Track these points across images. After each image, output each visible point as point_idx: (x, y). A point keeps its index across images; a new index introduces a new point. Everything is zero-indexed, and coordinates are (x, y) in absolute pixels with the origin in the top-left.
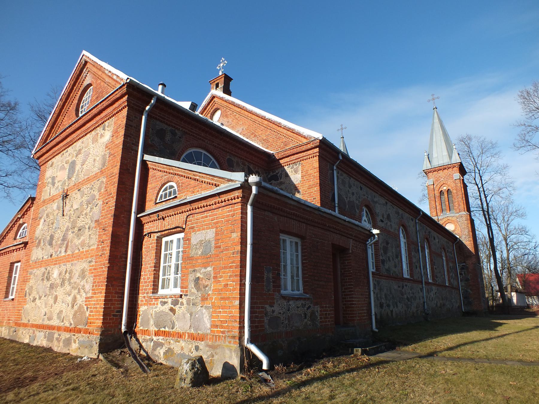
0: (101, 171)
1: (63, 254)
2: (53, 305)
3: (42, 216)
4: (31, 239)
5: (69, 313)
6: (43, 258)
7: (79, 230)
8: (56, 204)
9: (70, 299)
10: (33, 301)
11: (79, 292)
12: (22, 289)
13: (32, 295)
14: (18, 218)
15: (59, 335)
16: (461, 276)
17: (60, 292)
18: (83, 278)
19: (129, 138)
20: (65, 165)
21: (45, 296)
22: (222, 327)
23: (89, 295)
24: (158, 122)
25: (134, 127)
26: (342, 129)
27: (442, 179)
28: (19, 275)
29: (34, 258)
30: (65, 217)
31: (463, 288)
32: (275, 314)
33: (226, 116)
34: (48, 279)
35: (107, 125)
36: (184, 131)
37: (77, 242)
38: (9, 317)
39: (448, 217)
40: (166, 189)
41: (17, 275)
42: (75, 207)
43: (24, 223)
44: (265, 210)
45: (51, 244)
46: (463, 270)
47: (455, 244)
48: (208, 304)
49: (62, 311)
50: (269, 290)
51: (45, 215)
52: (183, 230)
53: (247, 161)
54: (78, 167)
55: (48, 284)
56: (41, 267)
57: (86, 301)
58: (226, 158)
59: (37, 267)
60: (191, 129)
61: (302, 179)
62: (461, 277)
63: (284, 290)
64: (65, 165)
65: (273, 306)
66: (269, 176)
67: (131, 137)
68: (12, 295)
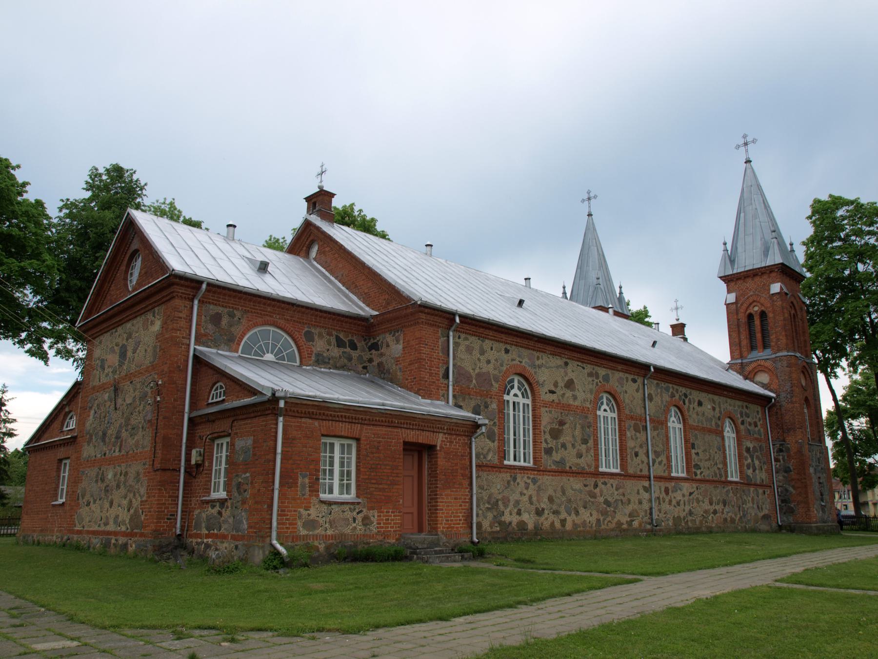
0: (152, 366)
1: (117, 454)
2: (109, 509)
3: (92, 406)
4: (80, 432)
5: (125, 516)
6: (95, 456)
7: (133, 429)
8: (107, 394)
9: (125, 502)
10: (87, 505)
11: (134, 495)
12: (73, 492)
13: (86, 498)
14: (64, 405)
15: (116, 540)
16: (778, 463)
17: (116, 496)
18: (138, 481)
19: (178, 332)
20: (116, 348)
21: (100, 500)
22: (255, 528)
23: (144, 499)
24: (212, 307)
25: (184, 318)
26: (589, 199)
27: (751, 293)
28: (69, 475)
29: (85, 454)
30: (118, 412)
31: (781, 484)
32: (311, 517)
33: (324, 253)
34: (103, 480)
35: (157, 312)
36: (245, 310)
37: (132, 442)
38: (60, 524)
39: (758, 360)
40: (217, 389)
41: (67, 474)
42: (129, 401)
43: (70, 412)
44: (301, 417)
45: (104, 440)
46: (781, 454)
47: (769, 409)
48: (246, 506)
49: (118, 515)
50: (304, 495)
51: (96, 405)
52: (229, 435)
53: (334, 329)
54: (129, 354)
55: (103, 486)
56: (94, 466)
57: (141, 505)
58: (304, 332)
59: (90, 467)
60: (254, 306)
61: (403, 351)
62: (777, 466)
63: (329, 493)
64: (116, 348)
65: (309, 510)
66: (370, 344)
67: (180, 330)
68: (61, 498)
